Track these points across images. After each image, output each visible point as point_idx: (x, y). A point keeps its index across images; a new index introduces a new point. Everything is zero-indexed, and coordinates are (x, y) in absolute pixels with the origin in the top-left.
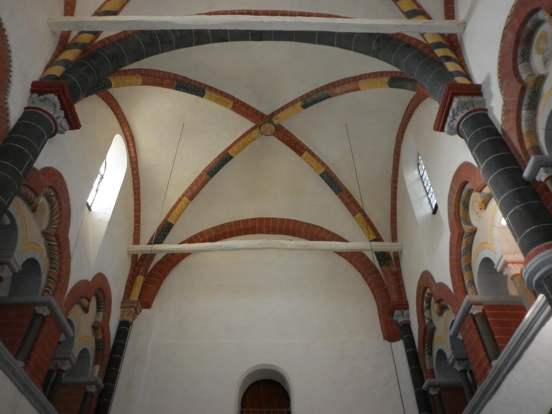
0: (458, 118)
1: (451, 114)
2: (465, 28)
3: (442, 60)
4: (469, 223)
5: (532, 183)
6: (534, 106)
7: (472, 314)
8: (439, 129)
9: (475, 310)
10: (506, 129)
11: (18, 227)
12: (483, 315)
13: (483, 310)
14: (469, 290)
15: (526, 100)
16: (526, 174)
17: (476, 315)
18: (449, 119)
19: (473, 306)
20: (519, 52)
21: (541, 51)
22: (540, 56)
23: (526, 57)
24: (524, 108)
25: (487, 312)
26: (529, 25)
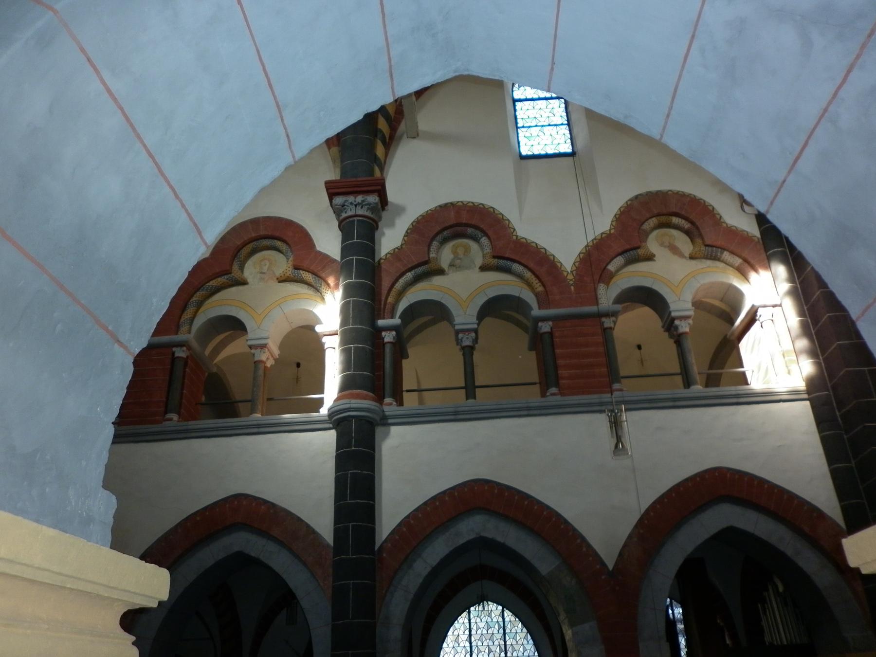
0: (360, 212)
1: (359, 198)
2: (414, 138)
3: (379, 136)
4: (242, 268)
5: (378, 332)
6: (417, 280)
7: (173, 353)
8: (330, 191)
9: (180, 353)
10: (383, 266)
11: (517, 295)
12: (185, 361)
13: (187, 357)
14: (184, 328)
15: (420, 270)
16: (381, 322)
17: (178, 357)
18: (351, 199)
19: (185, 348)
20: (445, 233)
21: (455, 252)
22: (452, 256)
23: (445, 241)
24: (413, 272)
25: (189, 362)
26: (470, 230)
